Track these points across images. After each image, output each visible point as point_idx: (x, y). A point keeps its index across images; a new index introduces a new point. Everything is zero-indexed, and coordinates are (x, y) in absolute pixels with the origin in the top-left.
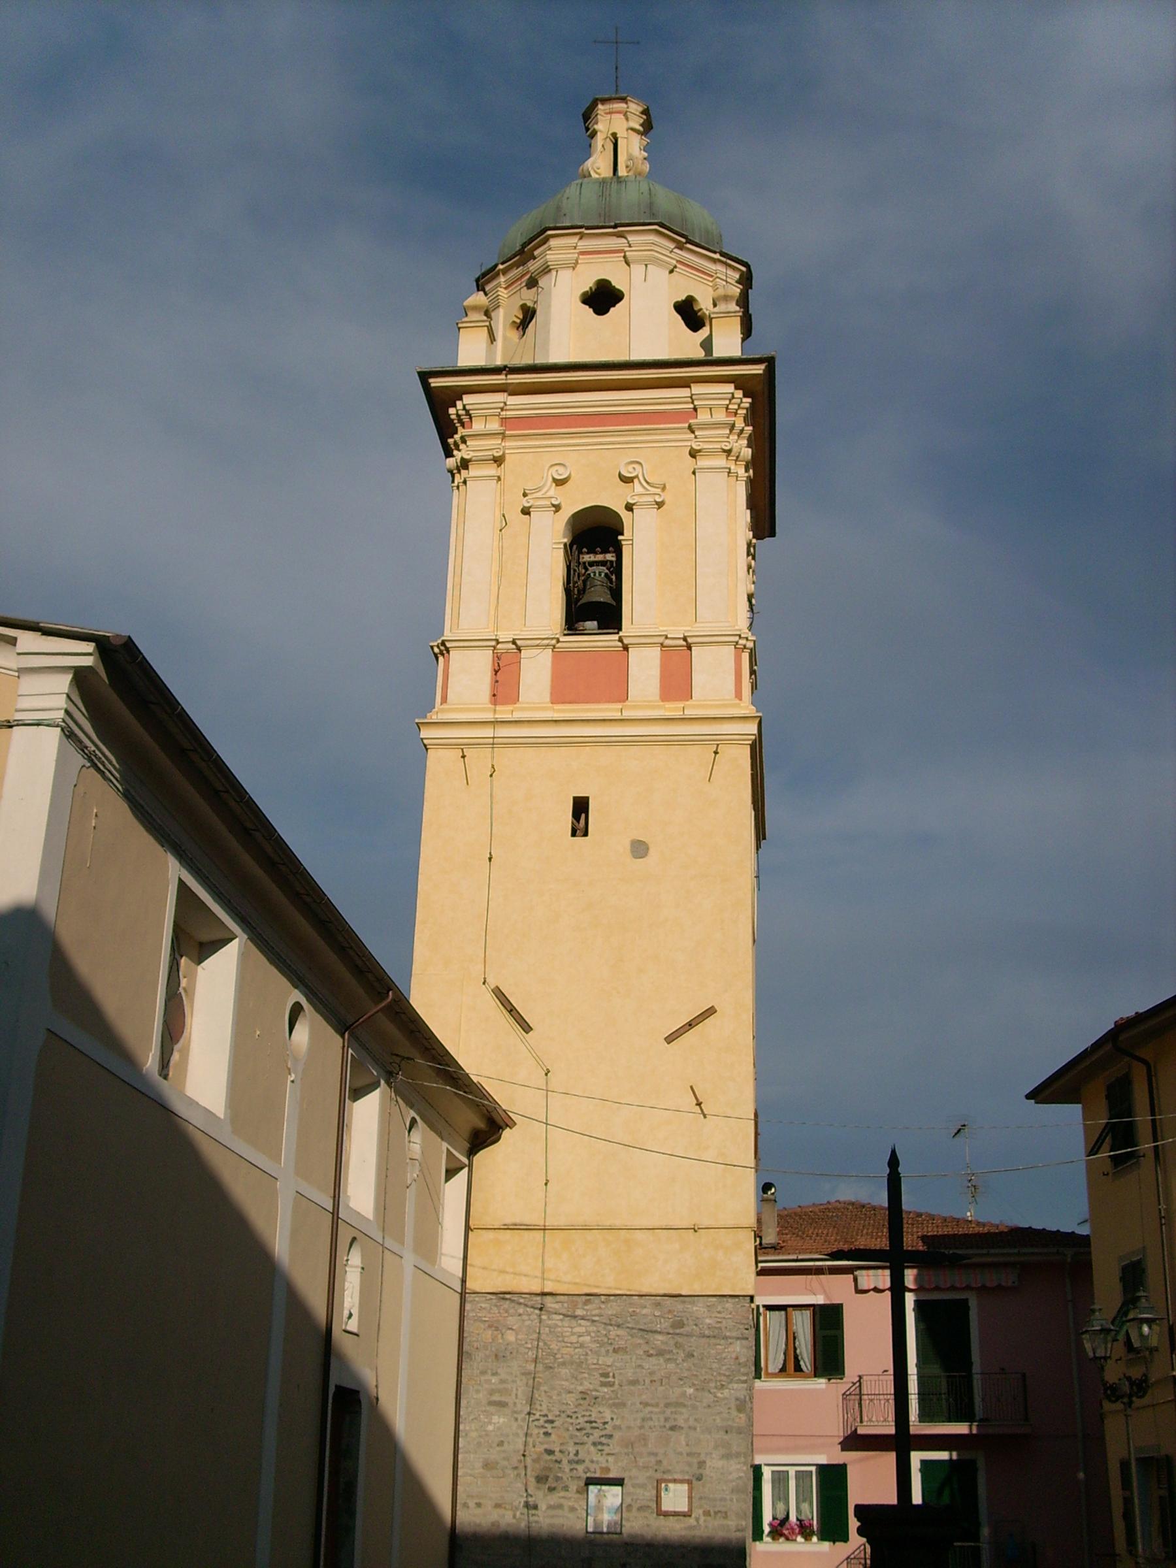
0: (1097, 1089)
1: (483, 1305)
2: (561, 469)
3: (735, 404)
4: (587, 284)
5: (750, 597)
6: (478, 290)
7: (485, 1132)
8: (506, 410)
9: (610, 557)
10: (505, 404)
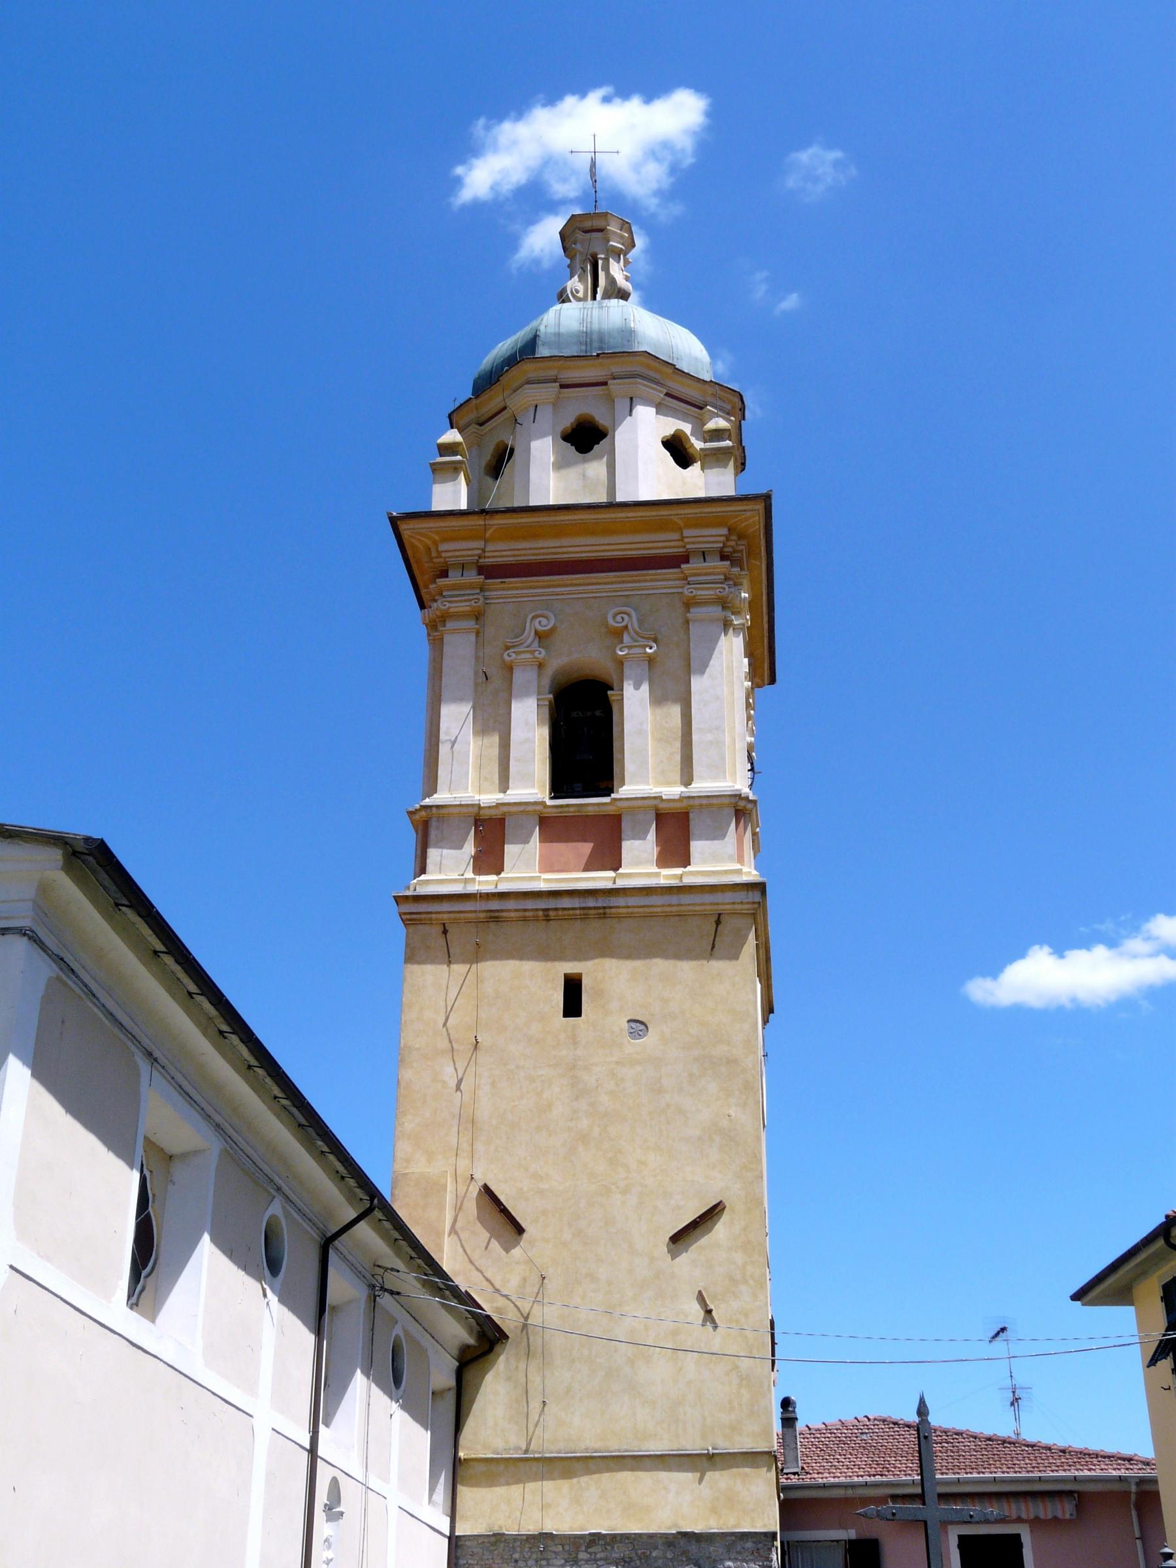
0: (1151, 1291)
1: (475, 1550)
2: (544, 621)
4: (567, 421)
5: (750, 749)
6: (452, 428)
7: (475, 1347)
8: (485, 557)
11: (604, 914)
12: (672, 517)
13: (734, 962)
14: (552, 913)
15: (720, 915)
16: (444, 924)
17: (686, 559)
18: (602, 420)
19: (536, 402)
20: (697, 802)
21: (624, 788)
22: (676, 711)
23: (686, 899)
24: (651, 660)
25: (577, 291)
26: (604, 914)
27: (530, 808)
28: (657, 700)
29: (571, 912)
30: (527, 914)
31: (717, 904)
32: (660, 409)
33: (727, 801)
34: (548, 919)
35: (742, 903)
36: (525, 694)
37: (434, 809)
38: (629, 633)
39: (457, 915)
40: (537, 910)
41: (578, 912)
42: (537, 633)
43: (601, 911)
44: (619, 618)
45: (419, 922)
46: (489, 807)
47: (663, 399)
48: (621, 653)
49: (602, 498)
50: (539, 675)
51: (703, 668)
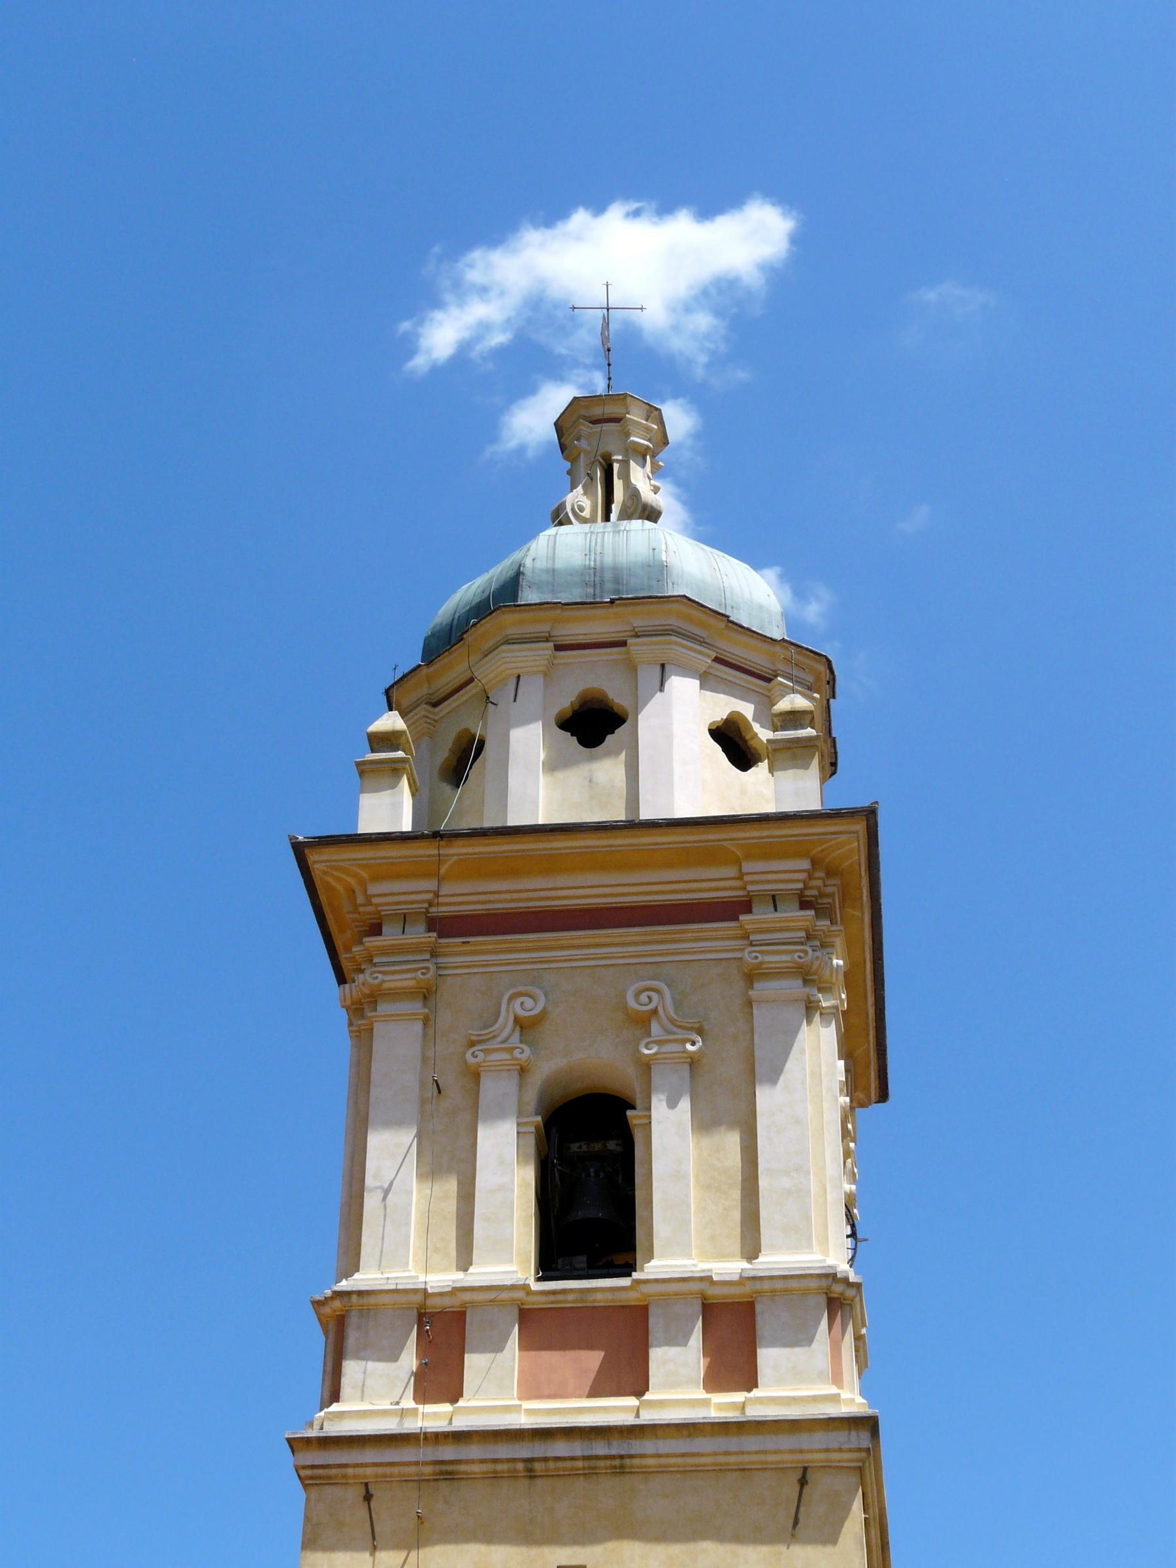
2: (529, 1002)
3: (819, 878)
4: (566, 700)
9: (612, 1145)
11: (622, 1467)
12: (724, 843)
13: (829, 1549)
14: (538, 1466)
15: (805, 1469)
16: (366, 1485)
17: (746, 906)
18: (617, 697)
19: (517, 672)
20: (766, 1286)
21: (653, 1263)
22: (732, 1141)
23: (751, 1443)
24: (693, 1062)
25: (582, 509)
26: (622, 1467)
27: (505, 1295)
28: (704, 1123)
29: (568, 1464)
30: (499, 1467)
31: (801, 1451)
32: (707, 681)
33: (814, 1284)
34: (531, 1475)
35: (840, 1450)
36: (499, 1115)
37: (354, 1298)
38: (660, 1023)
39: (388, 1470)
40: (514, 1460)
41: (580, 1464)
42: (517, 1020)
43: (617, 1462)
44: (644, 997)
45: (329, 1481)
46: (441, 1294)
47: (710, 667)
48: (646, 1052)
49: (617, 813)
50: (521, 1086)
51: (774, 1076)
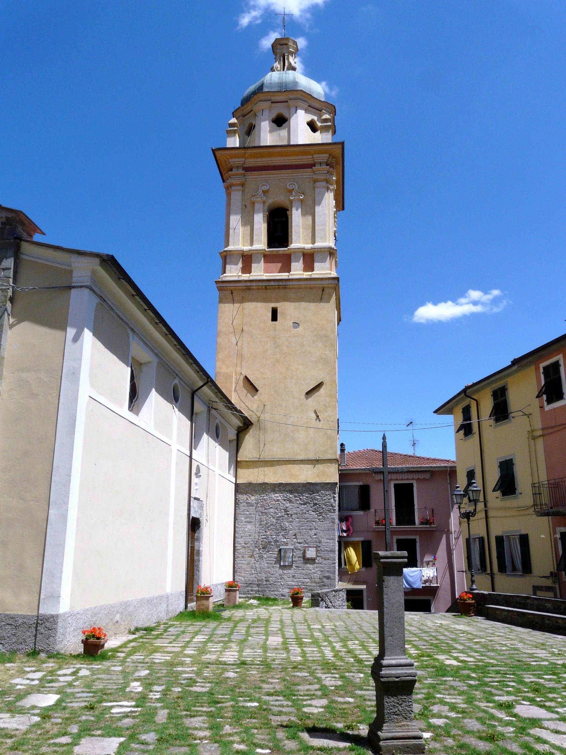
4: (274, 115)
10: (245, 162)
